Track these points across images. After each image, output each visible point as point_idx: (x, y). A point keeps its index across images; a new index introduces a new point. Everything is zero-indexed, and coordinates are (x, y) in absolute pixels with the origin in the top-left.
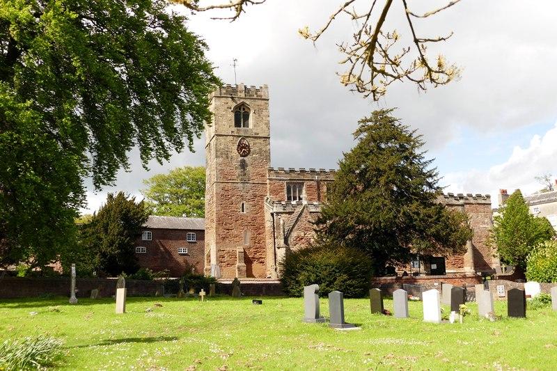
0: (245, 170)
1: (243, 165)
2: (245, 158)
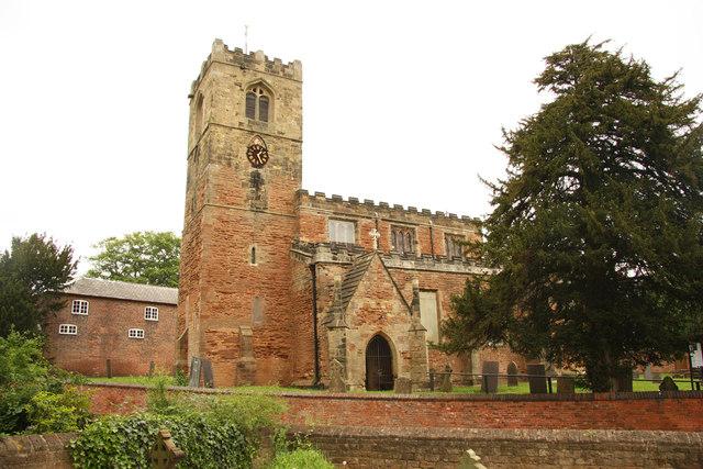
0: (258, 189)
1: (256, 181)
2: (260, 171)
